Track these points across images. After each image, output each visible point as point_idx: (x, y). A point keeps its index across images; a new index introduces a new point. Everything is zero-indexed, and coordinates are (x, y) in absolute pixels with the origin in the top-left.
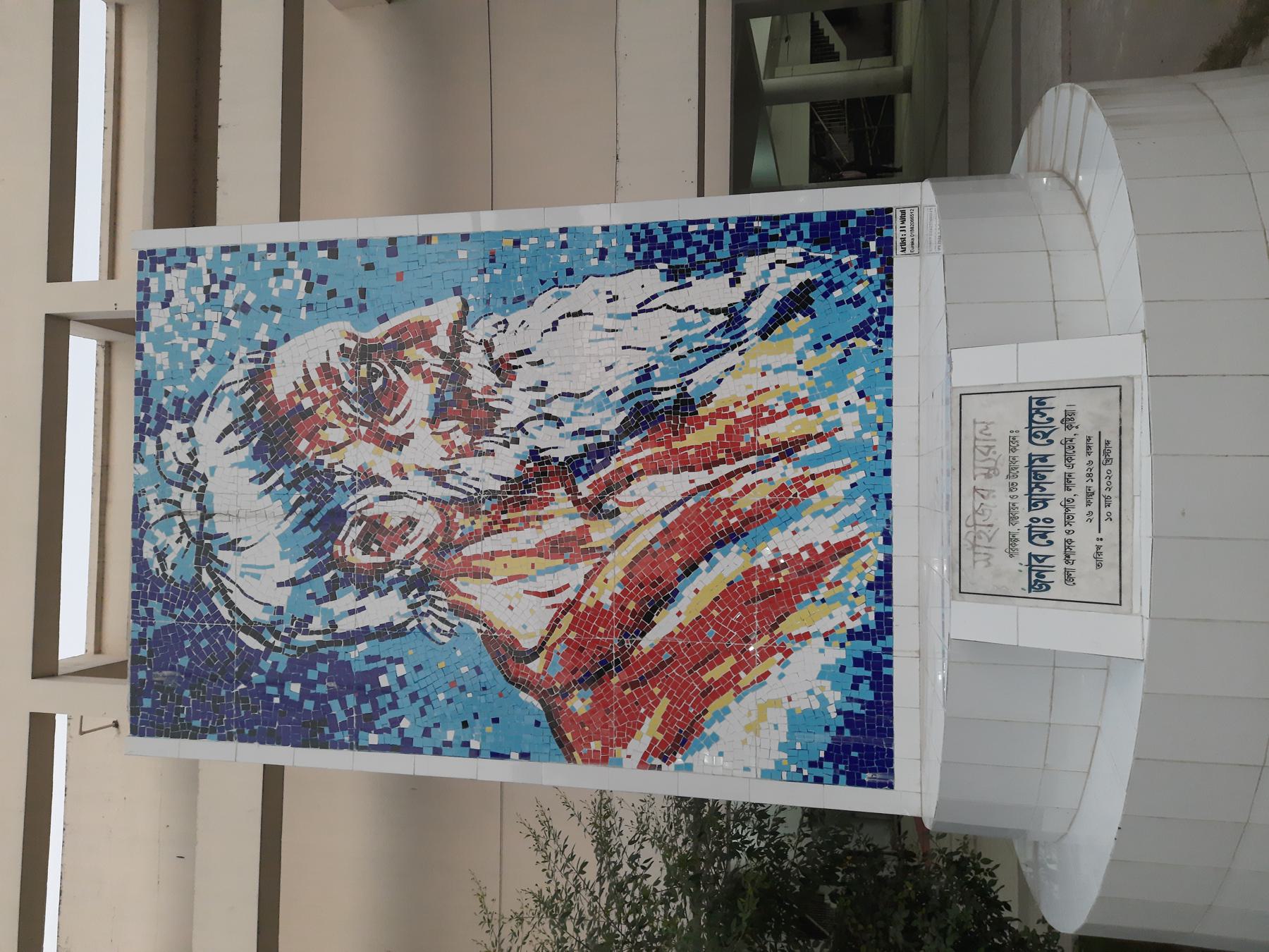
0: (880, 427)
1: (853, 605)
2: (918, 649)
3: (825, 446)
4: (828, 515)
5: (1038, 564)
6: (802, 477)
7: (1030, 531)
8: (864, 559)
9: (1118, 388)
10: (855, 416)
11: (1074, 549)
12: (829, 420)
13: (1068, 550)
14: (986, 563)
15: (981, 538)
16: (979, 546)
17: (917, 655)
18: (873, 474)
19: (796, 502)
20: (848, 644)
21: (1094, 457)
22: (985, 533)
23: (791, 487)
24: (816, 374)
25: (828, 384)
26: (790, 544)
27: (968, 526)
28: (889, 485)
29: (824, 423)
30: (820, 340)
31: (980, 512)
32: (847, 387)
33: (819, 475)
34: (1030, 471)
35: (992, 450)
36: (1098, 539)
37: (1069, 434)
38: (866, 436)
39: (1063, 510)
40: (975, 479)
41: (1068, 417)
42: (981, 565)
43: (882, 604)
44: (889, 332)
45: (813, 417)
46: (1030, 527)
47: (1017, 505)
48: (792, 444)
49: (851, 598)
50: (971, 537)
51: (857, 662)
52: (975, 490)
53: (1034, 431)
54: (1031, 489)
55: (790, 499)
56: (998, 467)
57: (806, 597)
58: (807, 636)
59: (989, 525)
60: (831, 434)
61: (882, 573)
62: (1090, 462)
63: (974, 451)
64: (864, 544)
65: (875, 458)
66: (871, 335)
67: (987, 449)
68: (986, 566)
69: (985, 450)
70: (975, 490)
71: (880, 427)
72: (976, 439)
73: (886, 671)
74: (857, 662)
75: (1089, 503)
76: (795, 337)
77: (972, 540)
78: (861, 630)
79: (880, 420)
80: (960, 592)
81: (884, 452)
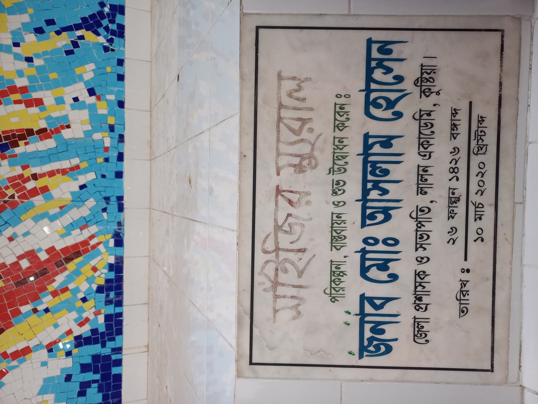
0: (112, 128)
1: (81, 311)
2: (146, 344)
3: (50, 143)
4: (53, 218)
5: (373, 311)
6: (21, 176)
7: (363, 259)
8: (93, 263)
9: (499, 34)
10: (85, 114)
11: (428, 287)
12: (55, 115)
13: (420, 288)
14: (293, 313)
15: (286, 271)
16: (283, 285)
17: (146, 349)
18: (104, 176)
19: (14, 205)
20: (75, 351)
21: (461, 141)
22: (293, 264)
23: (7, 188)
24: (38, 62)
25: (53, 76)
26: (6, 252)
27: (266, 252)
28: (121, 187)
29: (48, 119)
30: (43, 25)
31: (286, 228)
32: (75, 82)
33: (42, 175)
34: (365, 162)
35: (307, 126)
36: (463, 271)
37: (426, 104)
38: (97, 136)
39: (413, 225)
40: (278, 174)
41: (425, 75)
42: (285, 316)
43: (112, 306)
44: (120, 32)
45: (34, 110)
46: (364, 252)
47: (344, 217)
48: (6, 138)
49: (80, 303)
50: (270, 270)
51: (85, 368)
52: (279, 191)
53: (373, 96)
54: (365, 192)
55: (5, 202)
56: (316, 153)
57: (25, 309)
58: (27, 351)
59: (299, 251)
60: (57, 131)
61: (112, 275)
62: (456, 150)
63: (278, 126)
64: (94, 247)
65: (107, 160)
66: (101, 30)
67: (299, 123)
68: (294, 318)
69: (296, 125)
70: (279, 191)
71: (112, 128)
72: (281, 106)
73: (115, 370)
74: (85, 368)
75: (451, 215)
76: (9, 14)
77: (272, 274)
78: (90, 334)
79: (111, 121)
80: (251, 363)
81: (116, 154)
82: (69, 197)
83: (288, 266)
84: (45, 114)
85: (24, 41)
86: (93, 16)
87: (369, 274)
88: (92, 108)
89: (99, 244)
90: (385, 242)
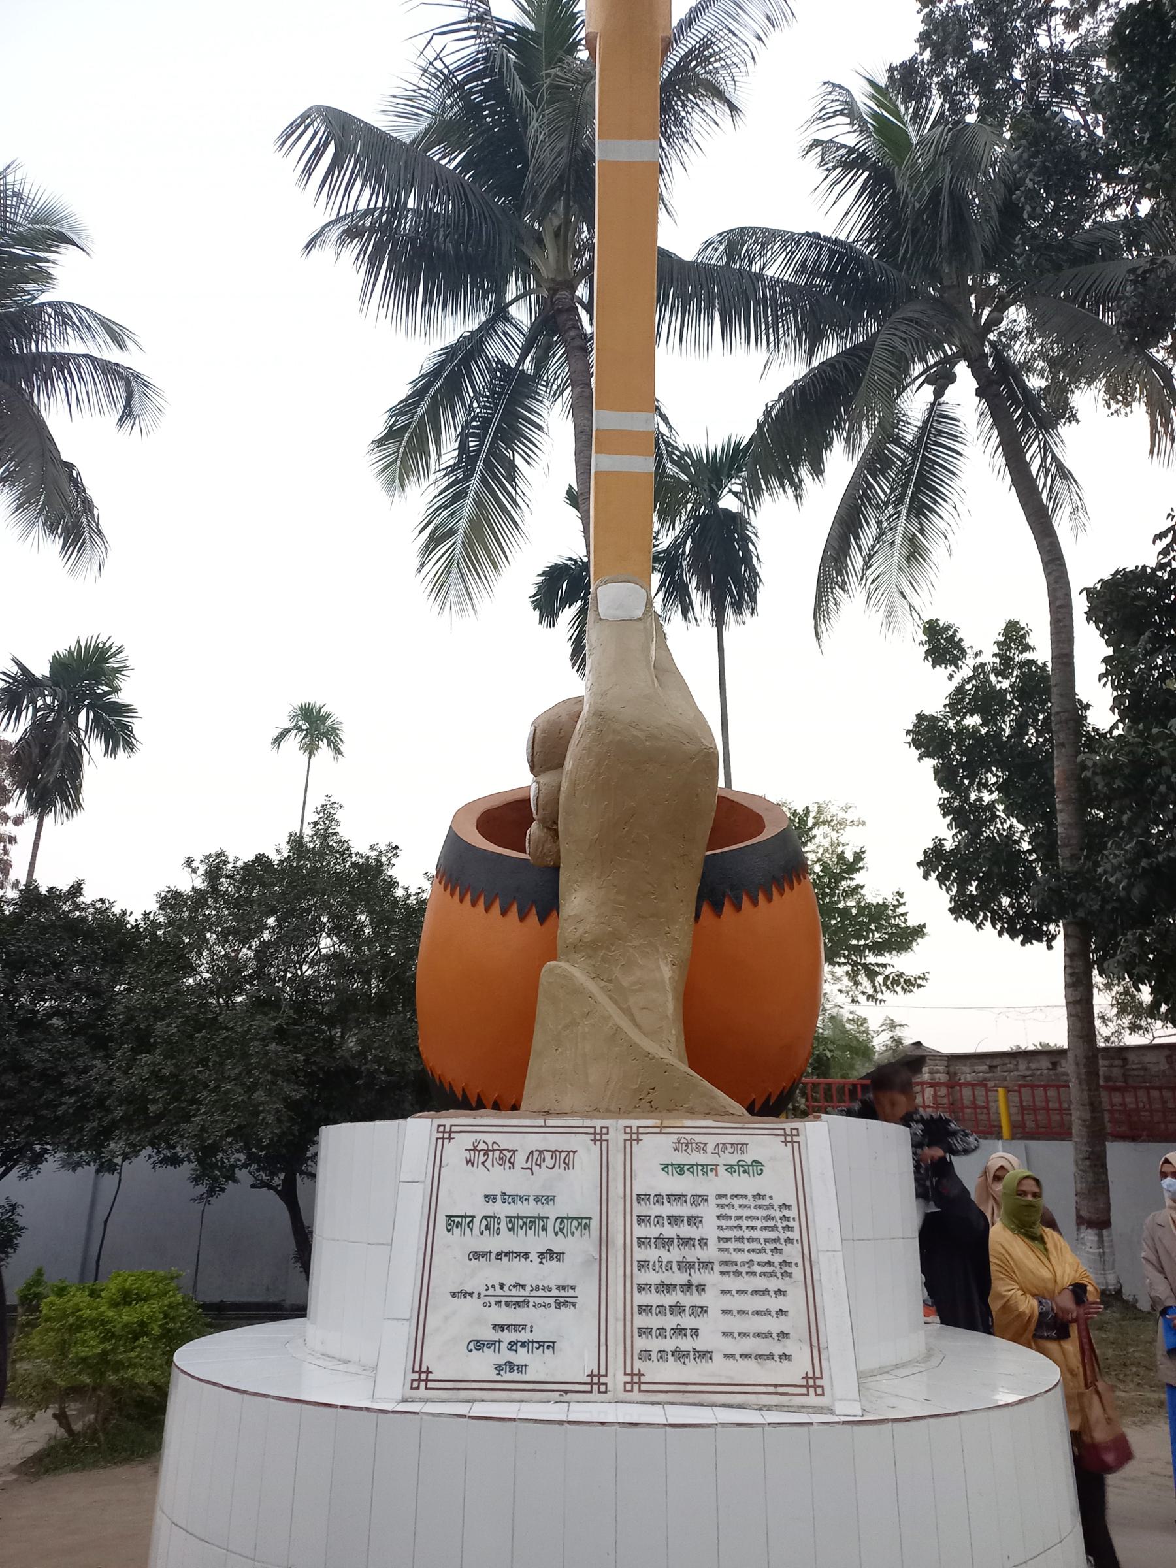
36: (479, 1294)
43: (695, 1283)
53: (565, 1221)
54: (522, 1218)
62: (550, 1289)
87: (484, 1220)
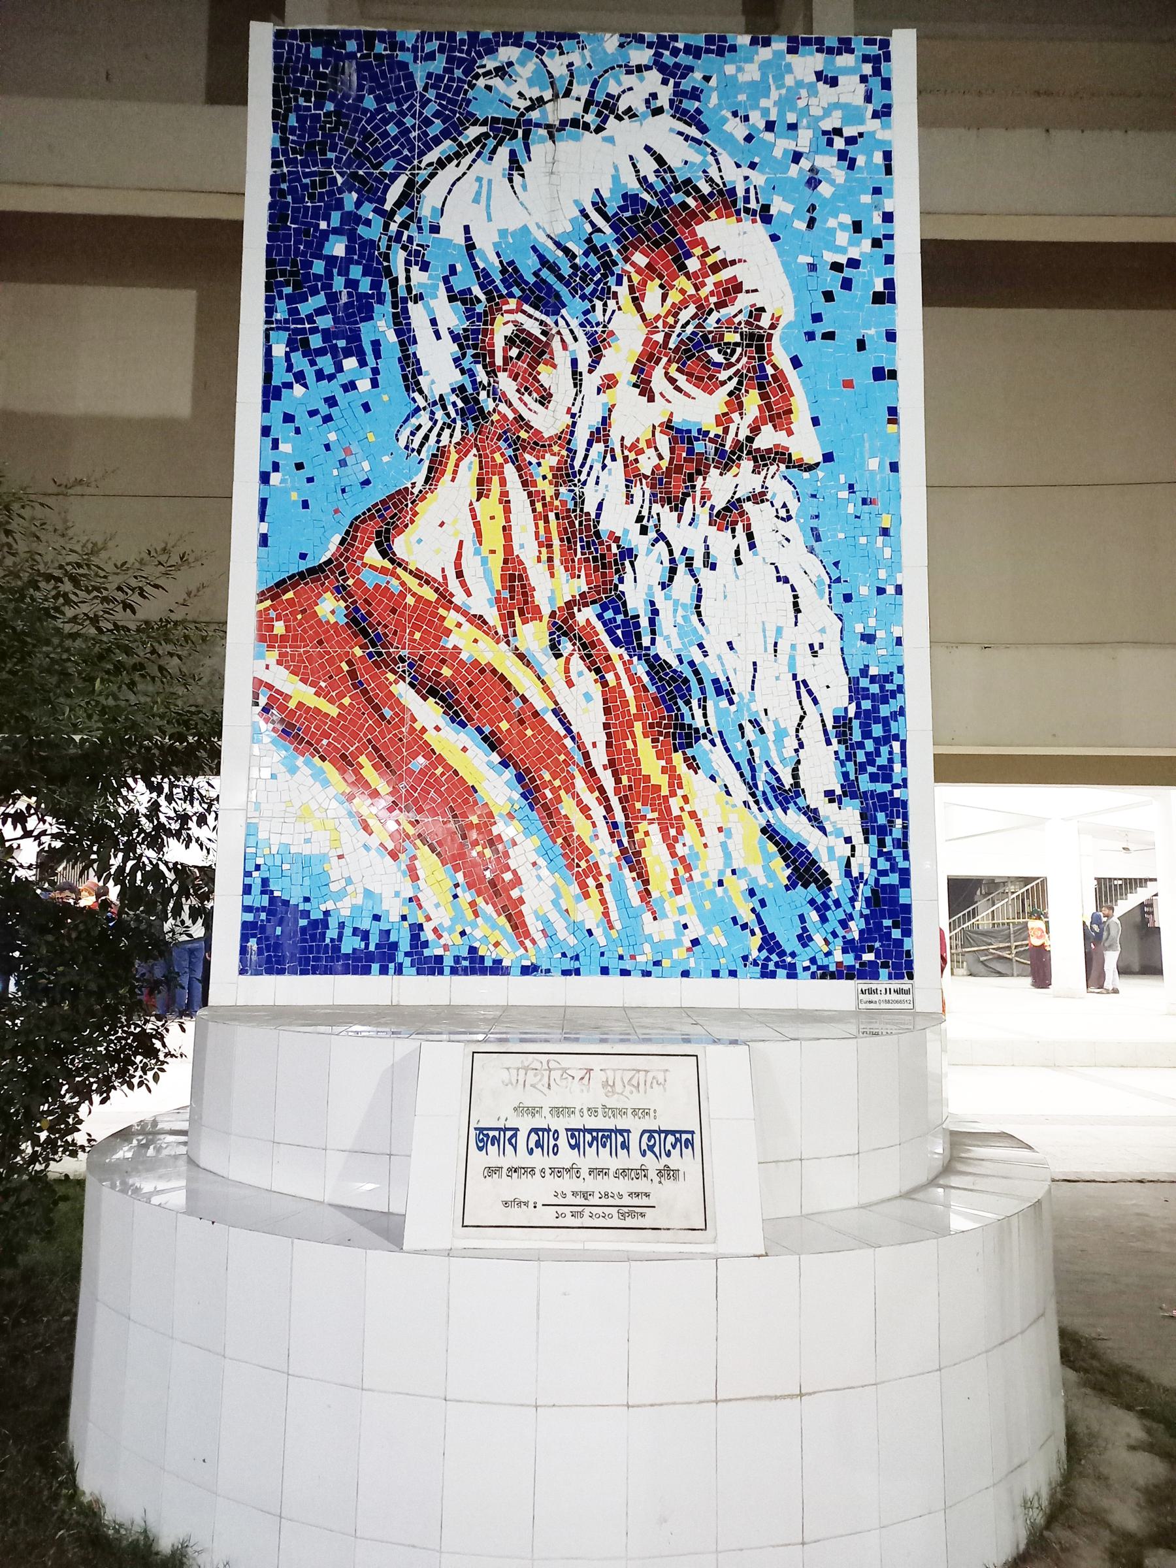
1: (451, 930)
3: (636, 901)
4: (555, 903)
7: (543, 1130)
10: (670, 935)
11: (524, 1177)
12: (666, 905)
14: (507, 1081)
15: (535, 1075)
18: (602, 954)
19: (570, 867)
23: (587, 861)
24: (719, 890)
27: (548, 1062)
28: (590, 973)
30: (759, 896)
31: (565, 1076)
33: (601, 893)
34: (611, 1131)
37: (652, 1174)
38: (647, 948)
39: (568, 1166)
46: (549, 1130)
50: (536, 1065)
53: (656, 1135)
54: (590, 1131)
57: (460, 876)
61: (488, 963)
62: (621, 1196)
64: (522, 943)
65: (621, 957)
66: (765, 953)
69: (634, 1082)
72: (647, 1071)
75: (574, 1194)
77: (533, 1066)
78: (423, 939)
79: (666, 963)
82: (579, 919)
83: (539, 1077)
84: (666, 896)
85: (739, 878)
86: (778, 944)
88: (678, 943)
89: (526, 949)
90: (556, 1145)
